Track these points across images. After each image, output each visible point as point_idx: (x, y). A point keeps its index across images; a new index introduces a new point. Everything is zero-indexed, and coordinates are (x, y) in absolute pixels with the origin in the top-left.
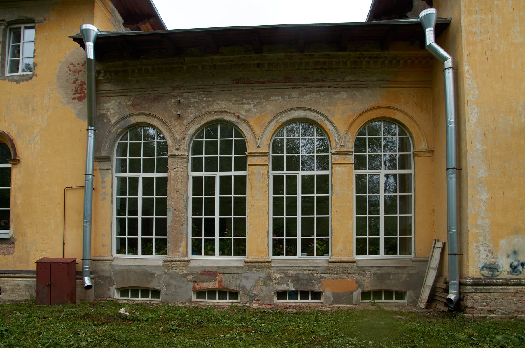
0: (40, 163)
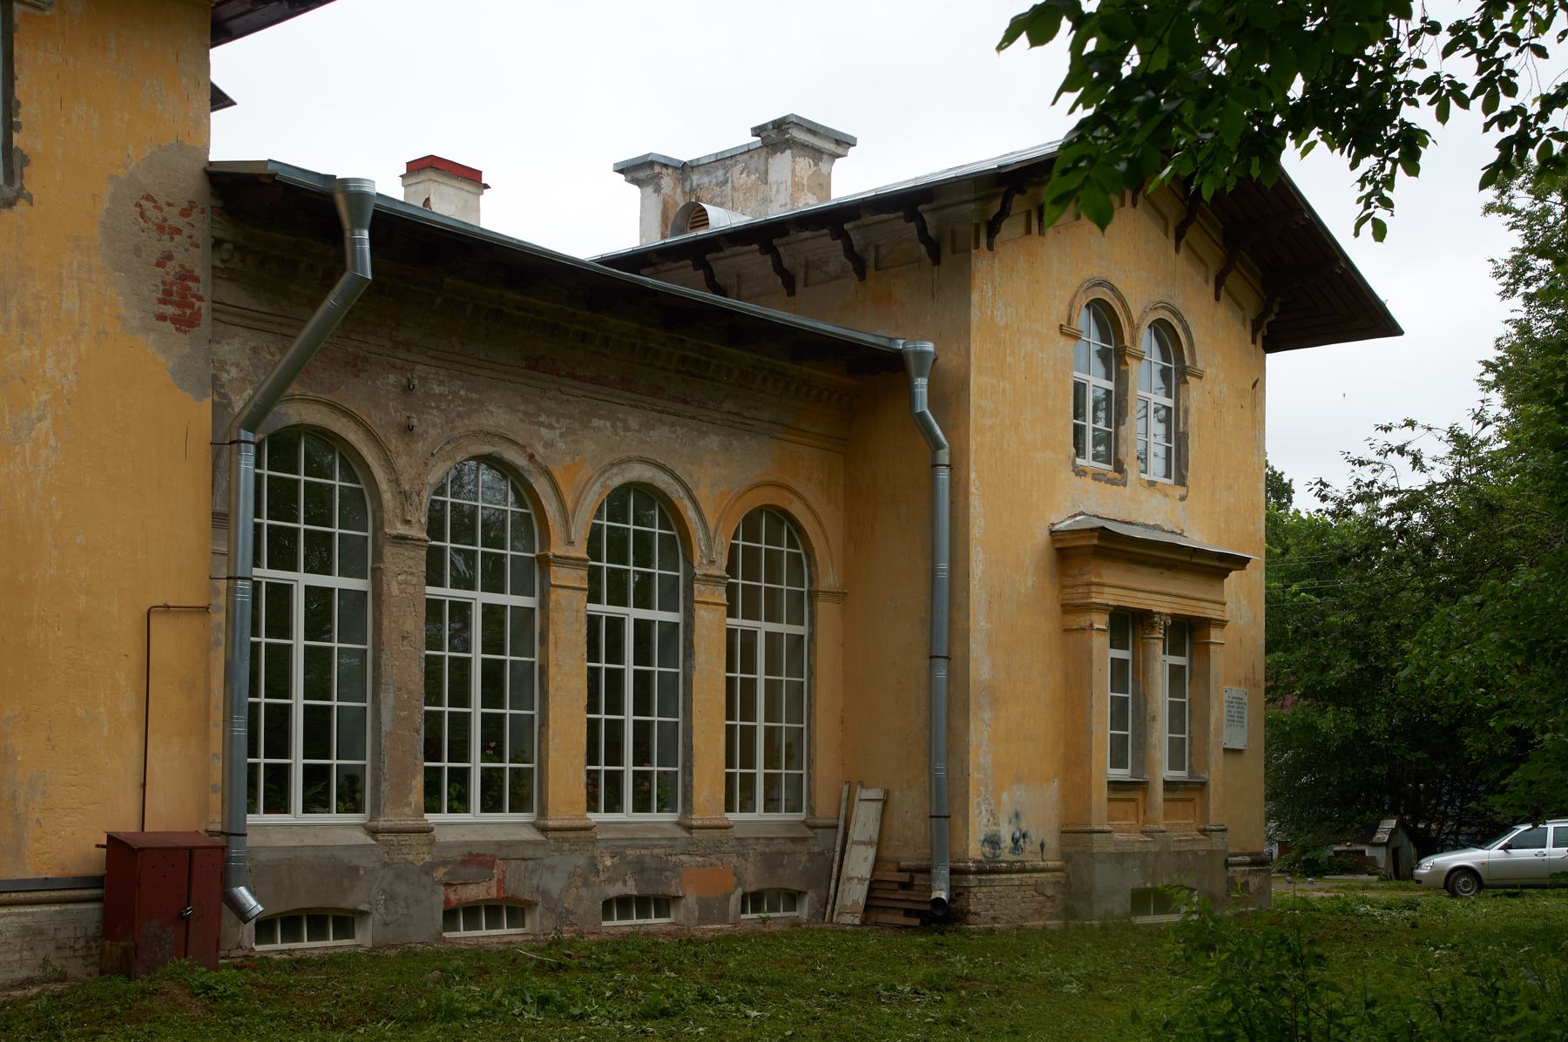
0: (58, 515)
